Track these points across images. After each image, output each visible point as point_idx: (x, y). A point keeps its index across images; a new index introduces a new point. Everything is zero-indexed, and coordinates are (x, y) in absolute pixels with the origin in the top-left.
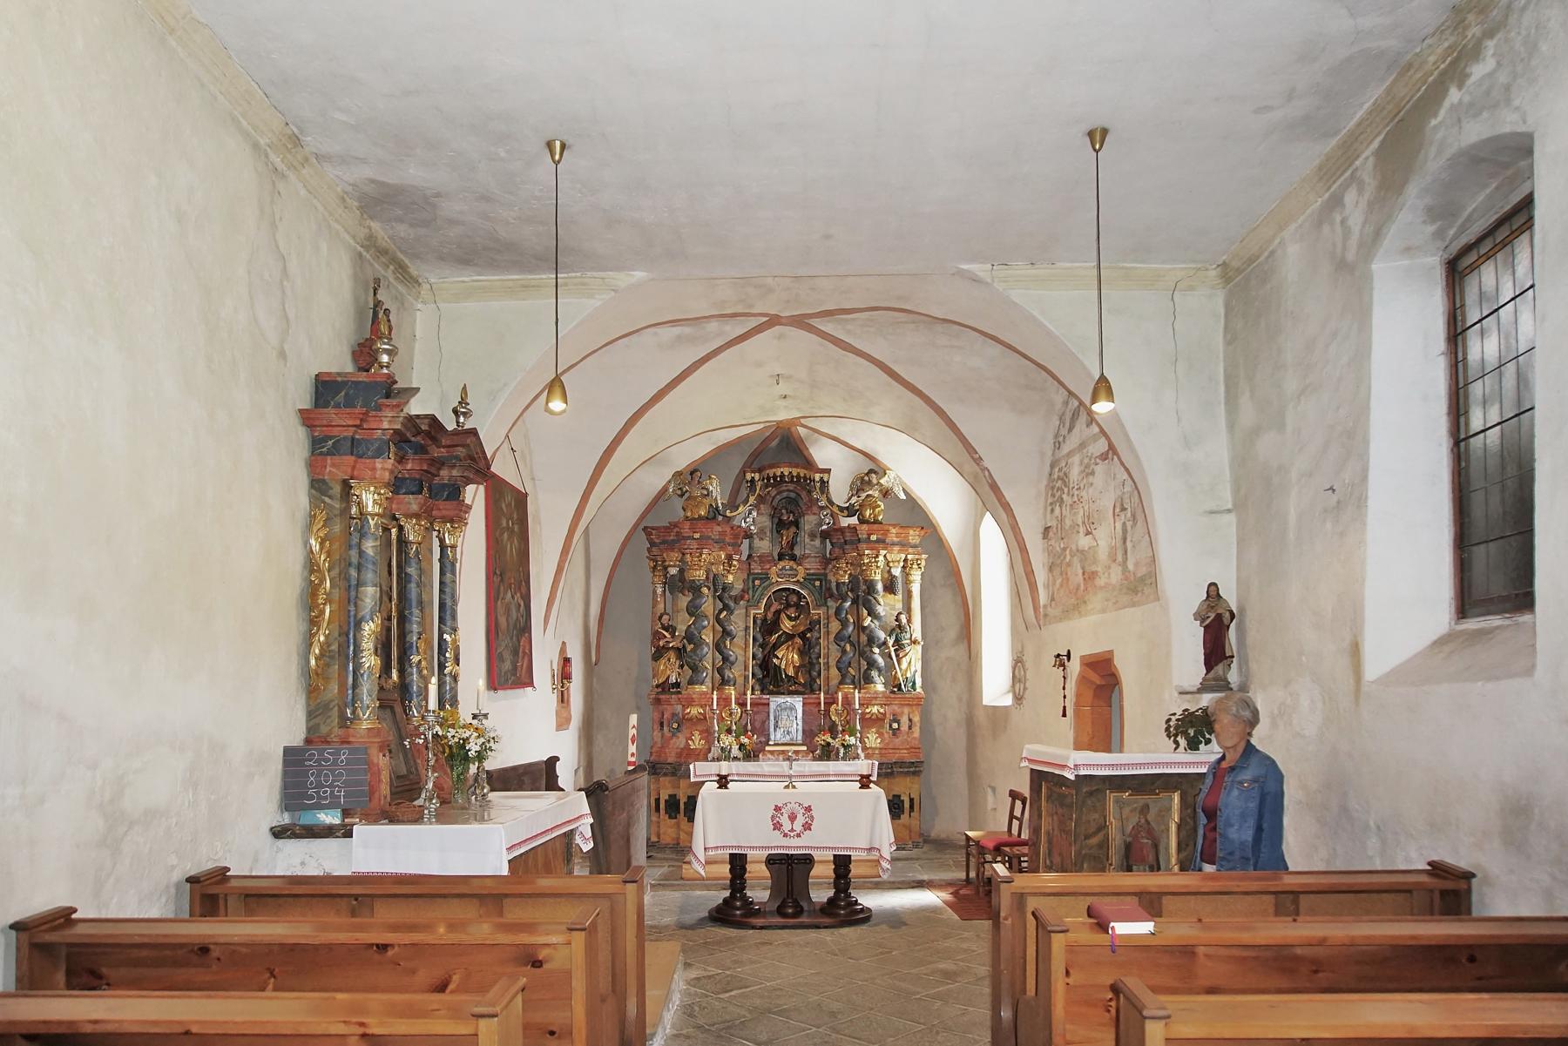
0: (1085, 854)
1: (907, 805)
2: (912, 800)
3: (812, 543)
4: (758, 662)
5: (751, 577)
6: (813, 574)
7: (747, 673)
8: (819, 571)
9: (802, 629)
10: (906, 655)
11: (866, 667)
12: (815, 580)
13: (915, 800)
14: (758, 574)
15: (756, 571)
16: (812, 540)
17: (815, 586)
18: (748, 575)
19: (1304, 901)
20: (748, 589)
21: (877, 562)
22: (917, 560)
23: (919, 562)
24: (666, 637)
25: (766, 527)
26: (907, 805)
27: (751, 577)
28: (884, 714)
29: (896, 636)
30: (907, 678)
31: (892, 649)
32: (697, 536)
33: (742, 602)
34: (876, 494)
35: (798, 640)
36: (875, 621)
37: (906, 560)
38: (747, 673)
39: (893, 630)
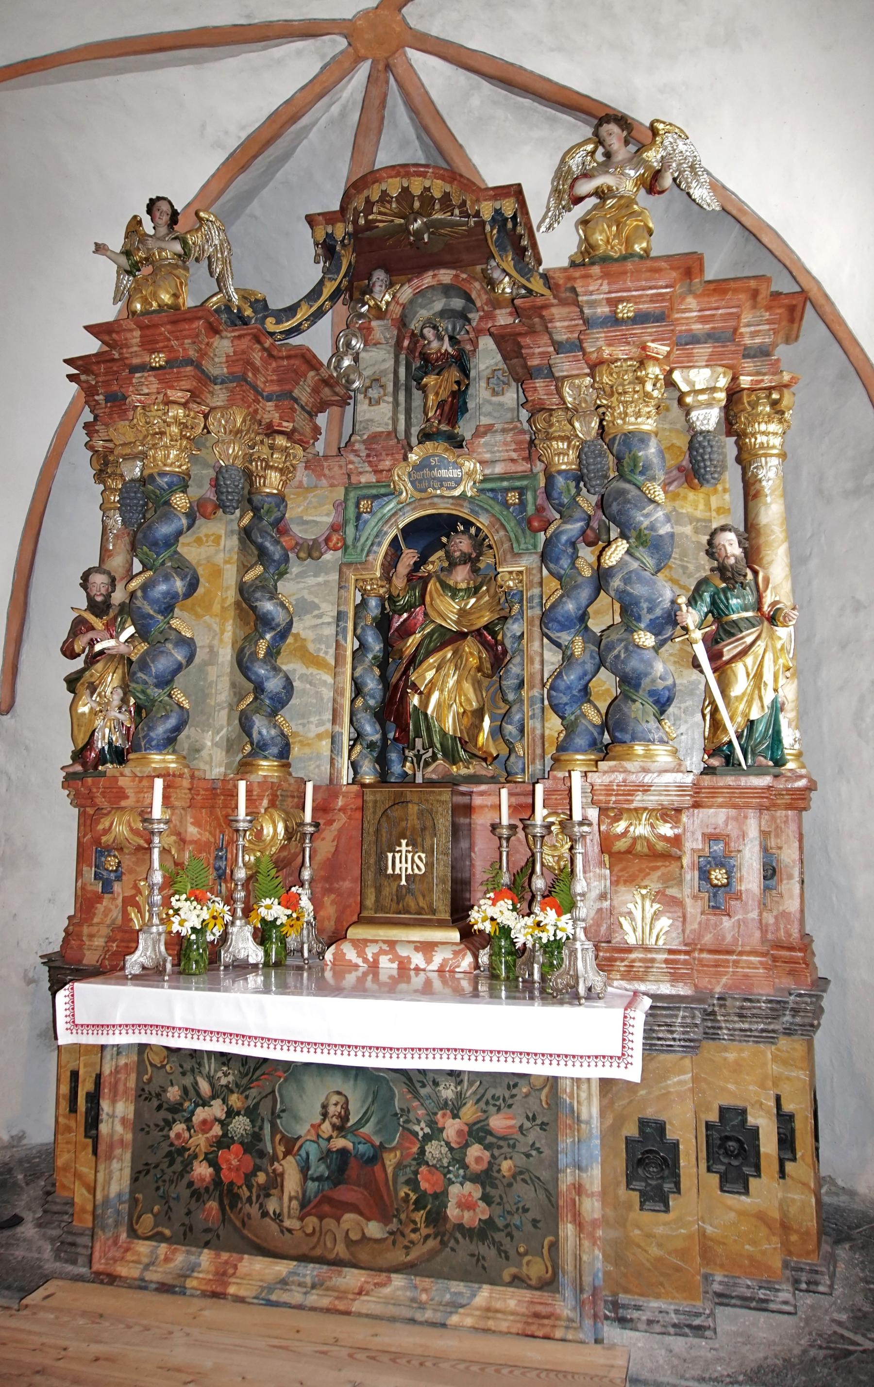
0: (724, 582)
1: (768, 1145)
2: (785, 1120)
3: (495, 399)
4: (372, 702)
5: (353, 495)
6: (501, 478)
7: (337, 728)
8: (513, 468)
9: (486, 618)
10: (744, 653)
11: (614, 691)
12: (507, 490)
13: (798, 1125)
14: (369, 486)
15: (363, 479)
16: (495, 393)
17: (506, 505)
18: (346, 489)
19: (343, 584)
20: (346, 522)
21: (641, 381)
22: (770, 389)
23: (775, 396)
24: (92, 628)
25: (384, 372)
26: (768, 1145)
27: (353, 495)
28: (676, 841)
29: (713, 597)
30: (156, 326)
31: (697, 635)
32: (158, 359)
33: (329, 556)
34: (627, 187)
35: (471, 649)
36: (642, 553)
37: (734, 394)
38: (337, 728)
39: (702, 583)
